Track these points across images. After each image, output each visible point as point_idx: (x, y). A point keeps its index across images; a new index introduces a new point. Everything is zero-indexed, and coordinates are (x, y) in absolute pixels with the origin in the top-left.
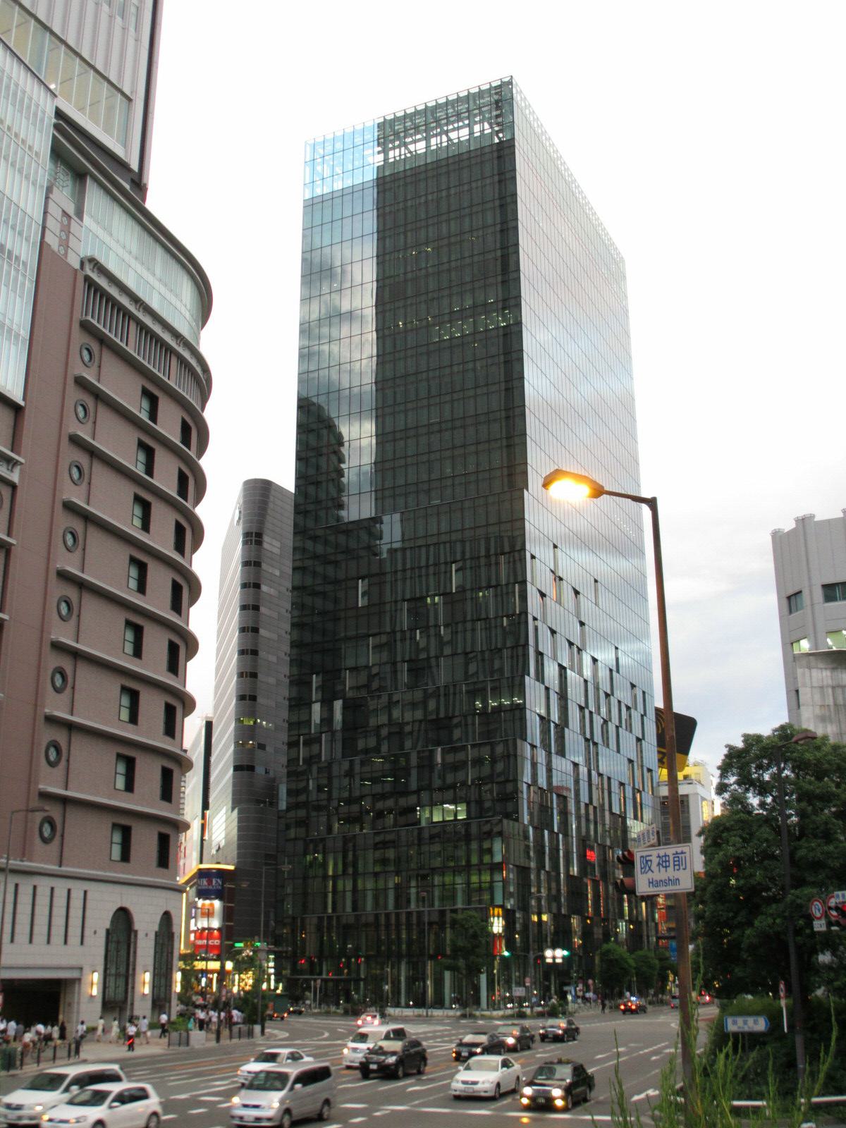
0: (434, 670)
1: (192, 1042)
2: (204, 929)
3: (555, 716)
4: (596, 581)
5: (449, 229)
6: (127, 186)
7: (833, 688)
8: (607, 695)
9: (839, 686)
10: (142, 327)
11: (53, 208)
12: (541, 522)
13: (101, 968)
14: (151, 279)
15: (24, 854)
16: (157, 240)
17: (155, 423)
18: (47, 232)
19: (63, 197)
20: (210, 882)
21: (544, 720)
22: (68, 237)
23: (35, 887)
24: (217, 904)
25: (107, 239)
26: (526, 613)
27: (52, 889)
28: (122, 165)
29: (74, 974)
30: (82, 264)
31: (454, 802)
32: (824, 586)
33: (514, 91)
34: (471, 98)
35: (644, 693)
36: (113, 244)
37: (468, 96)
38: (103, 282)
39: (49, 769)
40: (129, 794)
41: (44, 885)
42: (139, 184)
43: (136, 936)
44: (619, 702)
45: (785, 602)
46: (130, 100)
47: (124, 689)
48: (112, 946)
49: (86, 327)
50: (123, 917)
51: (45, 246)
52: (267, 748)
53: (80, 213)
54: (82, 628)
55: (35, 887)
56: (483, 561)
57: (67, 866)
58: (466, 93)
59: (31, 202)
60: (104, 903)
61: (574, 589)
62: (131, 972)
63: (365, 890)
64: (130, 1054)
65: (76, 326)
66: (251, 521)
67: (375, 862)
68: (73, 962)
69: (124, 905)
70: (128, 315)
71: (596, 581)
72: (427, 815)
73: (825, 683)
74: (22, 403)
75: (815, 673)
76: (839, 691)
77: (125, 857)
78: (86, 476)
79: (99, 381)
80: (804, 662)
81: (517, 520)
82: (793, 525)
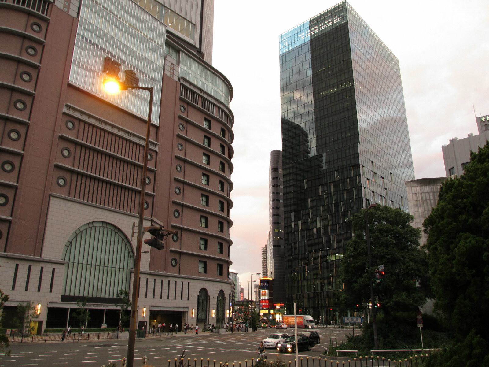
0: (331, 208)
1: (220, 332)
2: (263, 299)
4: (391, 174)
5: (330, 59)
6: (195, 53)
7: (421, 193)
10: (203, 98)
11: (167, 62)
13: (196, 308)
15: (165, 270)
16: (208, 69)
18: (165, 70)
19: (172, 58)
20: (264, 284)
22: (173, 71)
23: (169, 281)
24: (267, 291)
26: (361, 186)
28: (193, 47)
29: (186, 310)
30: (179, 79)
31: (339, 253)
32: (462, 164)
33: (347, 5)
34: (332, 11)
38: (187, 85)
40: (206, 251)
41: (173, 281)
42: (199, 51)
43: (209, 298)
45: (448, 172)
46: (195, 25)
47: (202, 217)
49: (181, 99)
50: (204, 292)
53: (178, 64)
54: (184, 196)
55: (169, 281)
56: (345, 169)
57: (182, 274)
58: (330, 9)
59: (159, 61)
60: (196, 287)
61: (381, 177)
63: (304, 285)
64: (196, 335)
65: (178, 100)
66: (274, 164)
67: (314, 275)
68: (186, 306)
69: (204, 287)
71: (391, 174)
72: (331, 258)
74: (159, 126)
75: (413, 188)
76: (424, 195)
77: (205, 272)
79: (187, 117)
80: (409, 184)
81: (356, 155)
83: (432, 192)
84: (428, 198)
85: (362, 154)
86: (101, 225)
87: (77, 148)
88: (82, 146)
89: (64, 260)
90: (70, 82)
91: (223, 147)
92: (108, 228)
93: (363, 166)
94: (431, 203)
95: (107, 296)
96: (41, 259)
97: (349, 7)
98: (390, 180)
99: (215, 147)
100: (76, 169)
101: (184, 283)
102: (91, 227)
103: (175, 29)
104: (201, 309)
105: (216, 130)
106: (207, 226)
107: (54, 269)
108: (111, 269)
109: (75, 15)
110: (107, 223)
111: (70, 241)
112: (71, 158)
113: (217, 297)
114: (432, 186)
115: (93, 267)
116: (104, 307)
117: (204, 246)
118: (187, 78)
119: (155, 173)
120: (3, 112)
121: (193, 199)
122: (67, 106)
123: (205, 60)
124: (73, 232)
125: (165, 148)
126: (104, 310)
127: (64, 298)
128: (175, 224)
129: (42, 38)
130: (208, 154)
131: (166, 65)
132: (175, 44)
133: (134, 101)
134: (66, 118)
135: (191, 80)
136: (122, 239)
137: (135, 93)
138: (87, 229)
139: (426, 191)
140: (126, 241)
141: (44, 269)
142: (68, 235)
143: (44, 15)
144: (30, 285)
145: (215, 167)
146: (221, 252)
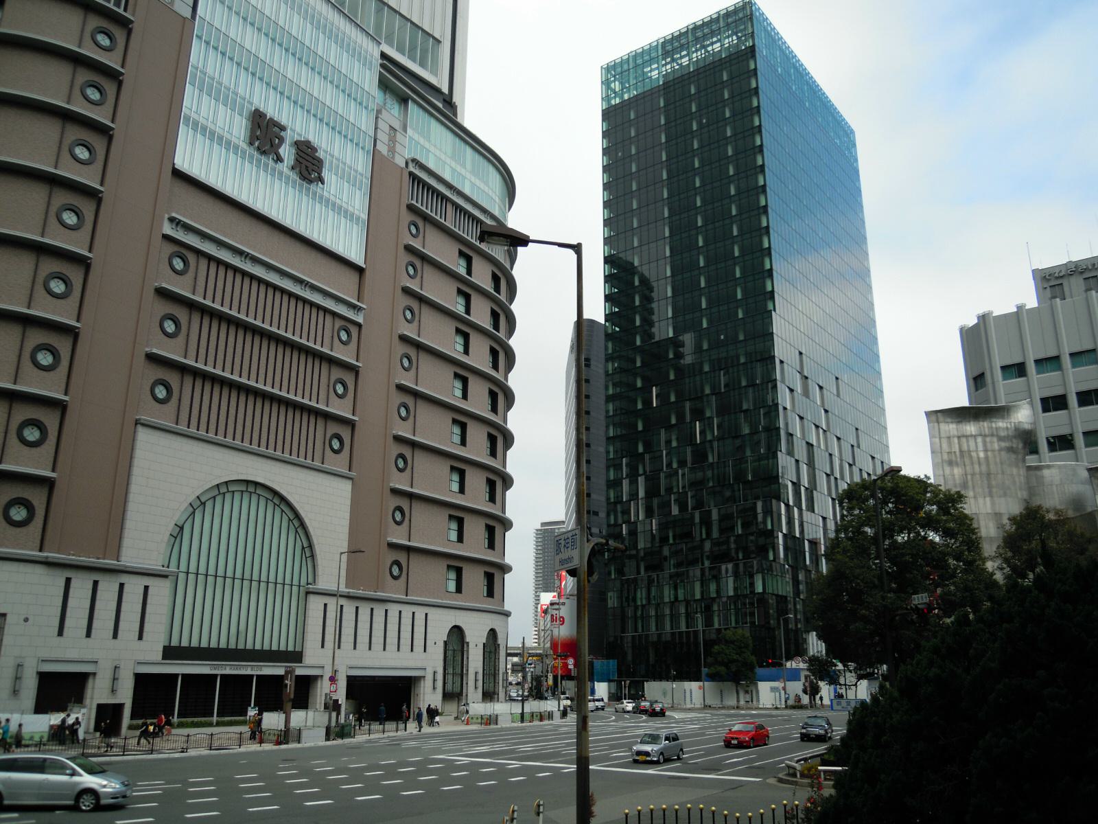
3: (805, 481)
6: (440, 105)
7: (959, 437)
8: (850, 465)
9: (964, 436)
10: (457, 207)
11: (381, 124)
12: (788, 334)
14: (463, 172)
17: (471, 276)
19: (393, 112)
21: (796, 485)
22: (395, 145)
23: (386, 611)
25: (427, 145)
27: (400, 612)
28: (436, 90)
30: (407, 163)
35: (882, 462)
36: (432, 149)
37: (718, 17)
39: (397, 527)
41: (393, 609)
42: (449, 102)
43: (468, 646)
44: (861, 470)
45: (972, 382)
46: (439, 42)
47: (453, 468)
48: (450, 653)
49: (411, 208)
50: (457, 632)
51: (376, 151)
52: (600, 514)
55: (386, 611)
59: (365, 122)
60: (441, 623)
62: (464, 672)
65: (404, 208)
68: (419, 665)
69: (457, 624)
70: (444, 198)
73: (952, 434)
77: (459, 589)
78: (417, 319)
82: (975, 321)
83: (981, 435)
84: (972, 447)
85: (779, 335)
86: (244, 488)
87: (192, 316)
88: (204, 311)
89: (168, 567)
90: (176, 167)
91: (495, 316)
92: (259, 495)
93: (782, 362)
94: (978, 458)
95: (204, 644)
96: (119, 565)
97: (758, 14)
98: (835, 392)
99: (481, 315)
100: (191, 363)
101: (328, 606)
102: (224, 494)
103: (397, 50)
104: (450, 671)
105: (482, 276)
106: (462, 490)
107: (146, 588)
108: (213, 581)
109: (187, 13)
110: (256, 484)
111: (180, 524)
112: (181, 339)
113: (445, 642)
114: (981, 423)
115: (220, 580)
116: (231, 669)
117: (456, 532)
118: (423, 161)
119: (357, 373)
120: (33, 234)
121: (435, 430)
122: (172, 220)
123: (459, 120)
124: (186, 504)
125: (382, 317)
126: (252, 676)
127: (171, 653)
128: (397, 486)
129: (116, 63)
130: (465, 330)
131: (379, 131)
132: (400, 84)
133: (313, 209)
134: (170, 249)
135: (431, 165)
136: (290, 519)
137: (315, 194)
138: (214, 497)
139: (969, 433)
140: (296, 523)
141: (150, 591)
142: (176, 510)
143: (121, 11)
144: (95, 624)
145: (479, 358)
146: (491, 545)
